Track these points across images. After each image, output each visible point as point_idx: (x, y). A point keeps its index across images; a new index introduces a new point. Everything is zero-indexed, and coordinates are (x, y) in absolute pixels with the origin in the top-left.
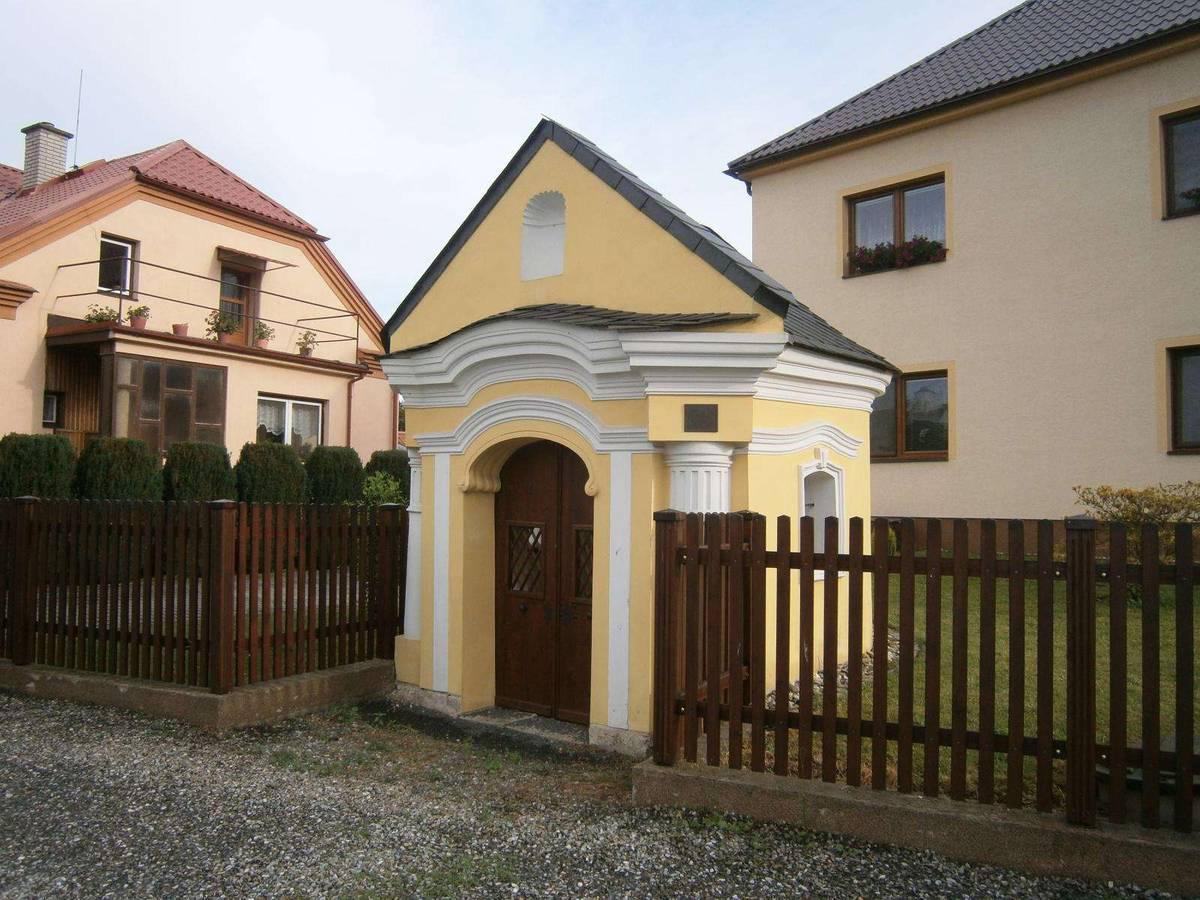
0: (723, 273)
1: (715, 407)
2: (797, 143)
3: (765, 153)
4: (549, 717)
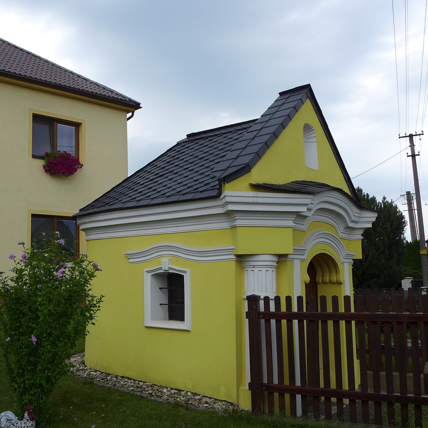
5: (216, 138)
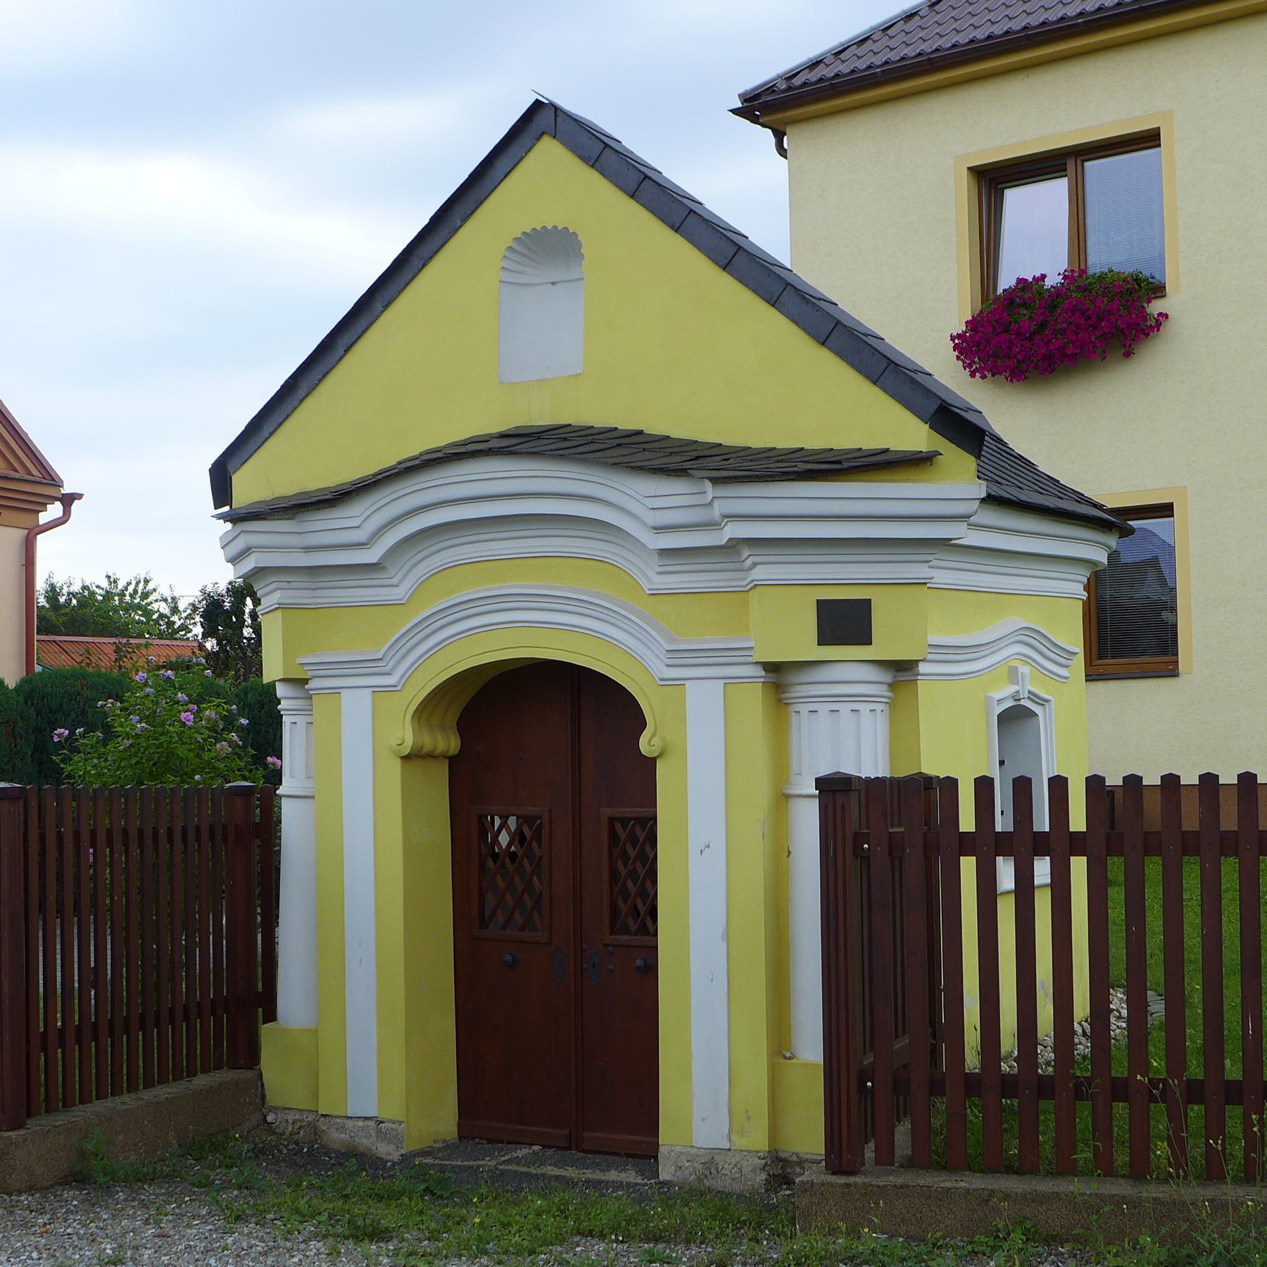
0: (875, 383)
1: (867, 603)
2: (878, 60)
3: (813, 76)
4: (566, 1149)
5: (677, 194)
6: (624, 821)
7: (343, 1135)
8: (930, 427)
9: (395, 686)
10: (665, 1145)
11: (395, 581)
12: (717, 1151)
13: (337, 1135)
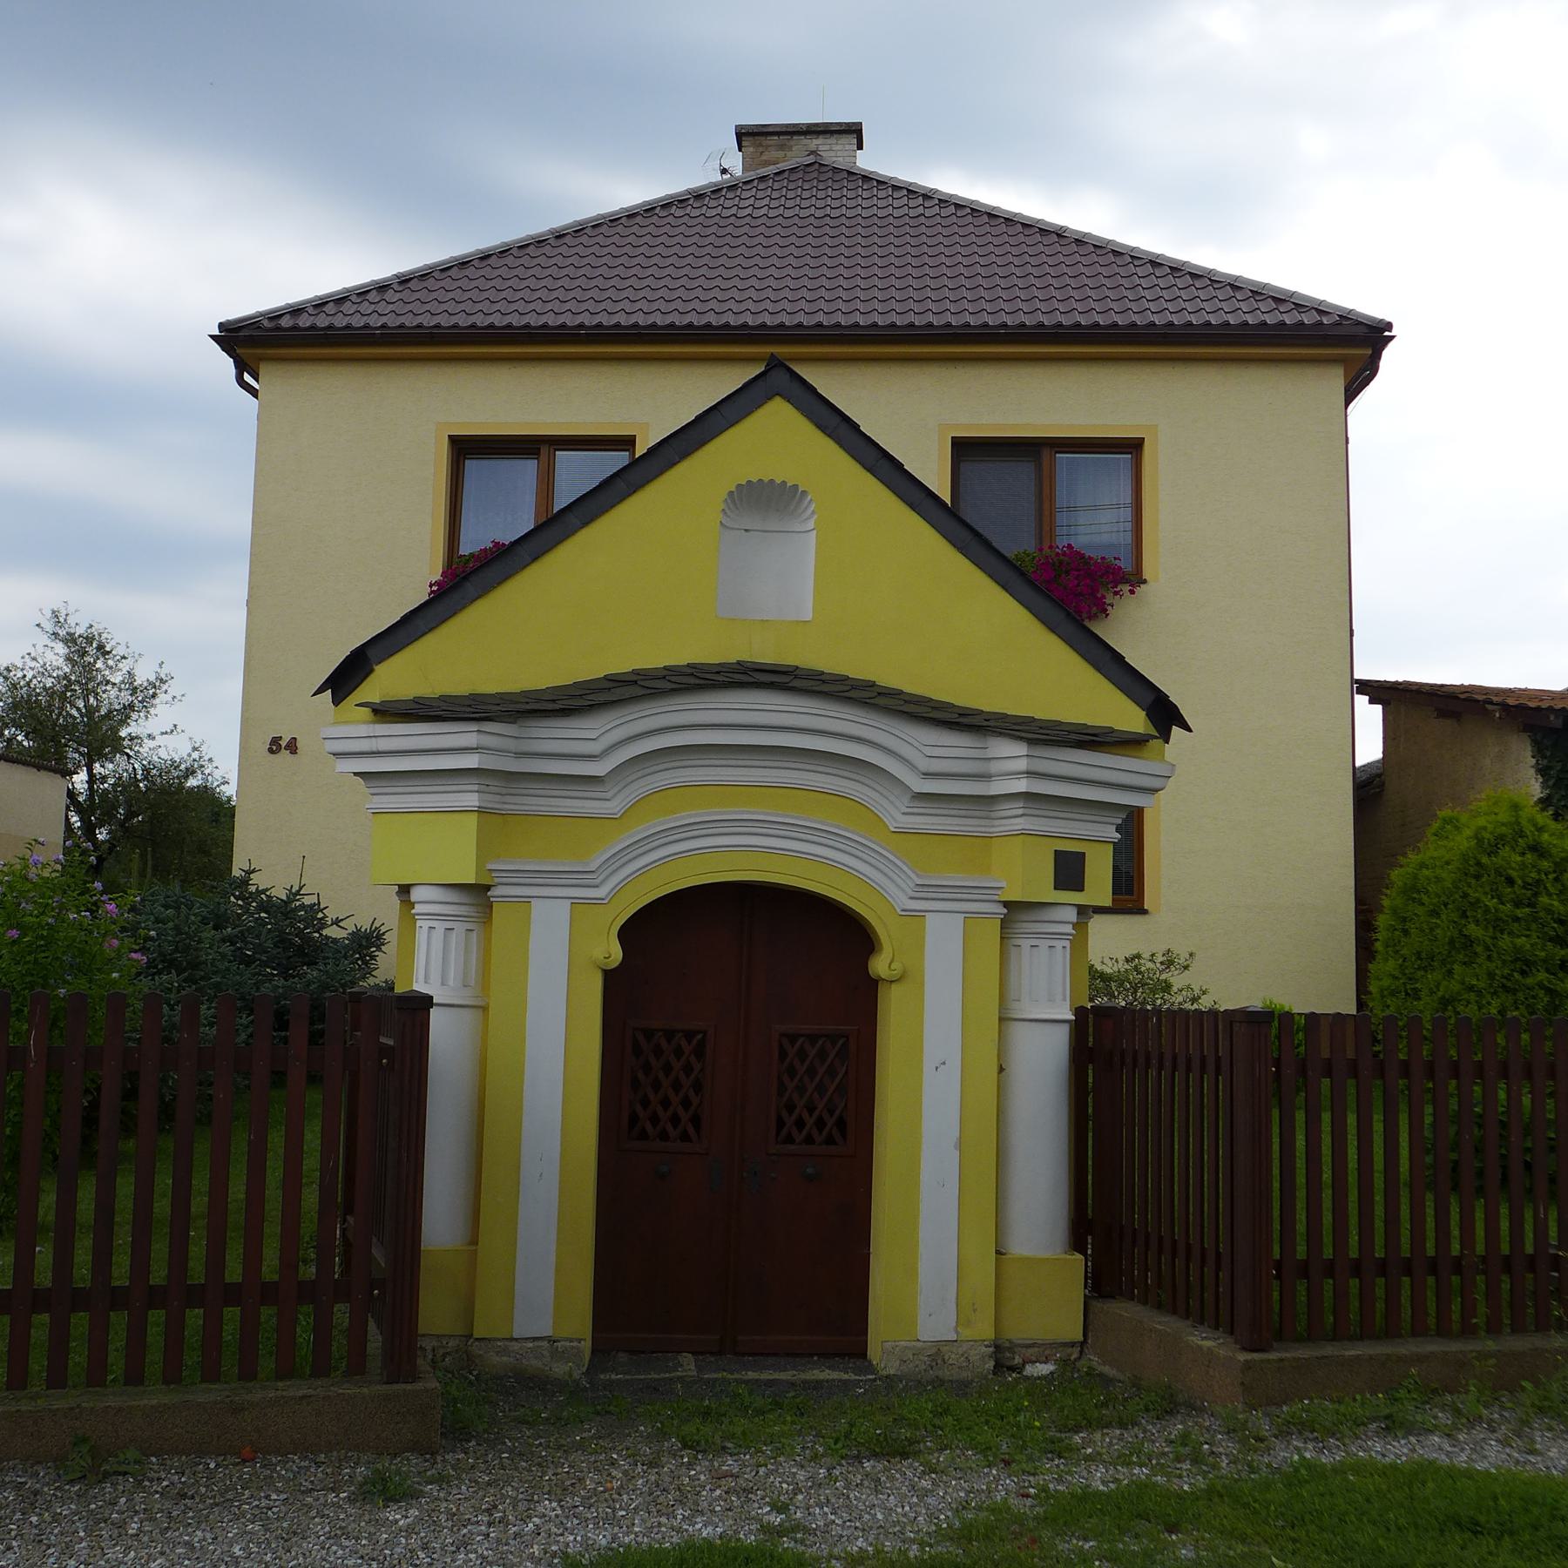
6: (793, 1038)
7: (505, 1359)
8: (1147, 715)
9: (603, 899)
10: (888, 1341)
11: (608, 795)
12: (944, 1343)
13: (498, 1359)
